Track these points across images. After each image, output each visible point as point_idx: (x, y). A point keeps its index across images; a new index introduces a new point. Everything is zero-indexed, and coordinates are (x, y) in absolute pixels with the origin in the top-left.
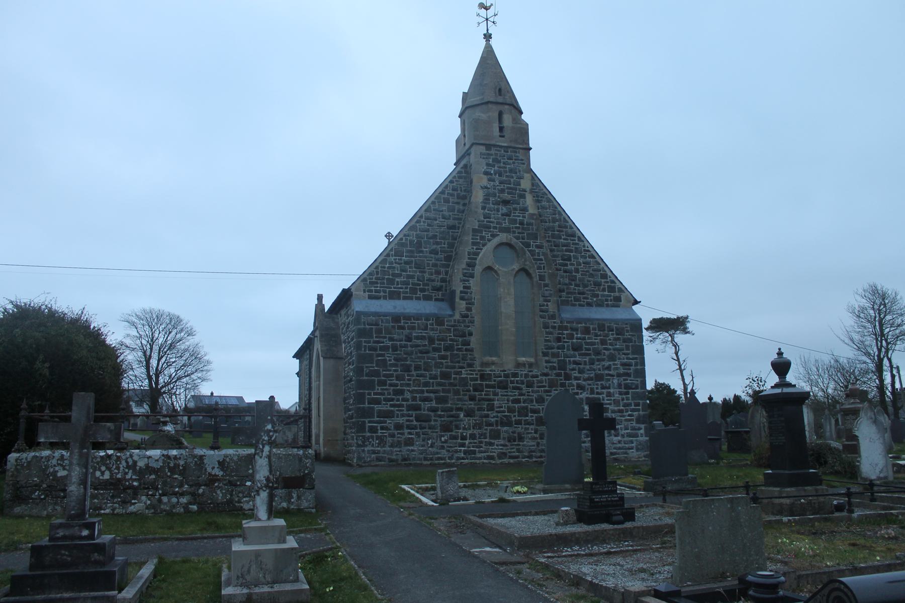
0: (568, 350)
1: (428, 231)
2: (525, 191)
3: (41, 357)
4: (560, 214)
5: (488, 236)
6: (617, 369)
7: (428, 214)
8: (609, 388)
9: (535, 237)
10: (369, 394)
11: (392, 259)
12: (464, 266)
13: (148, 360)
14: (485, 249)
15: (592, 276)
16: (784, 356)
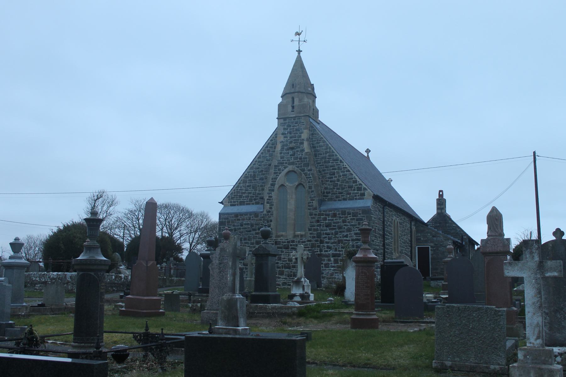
0: (323, 227)
1: (258, 168)
7: (259, 160)
12: (269, 186)
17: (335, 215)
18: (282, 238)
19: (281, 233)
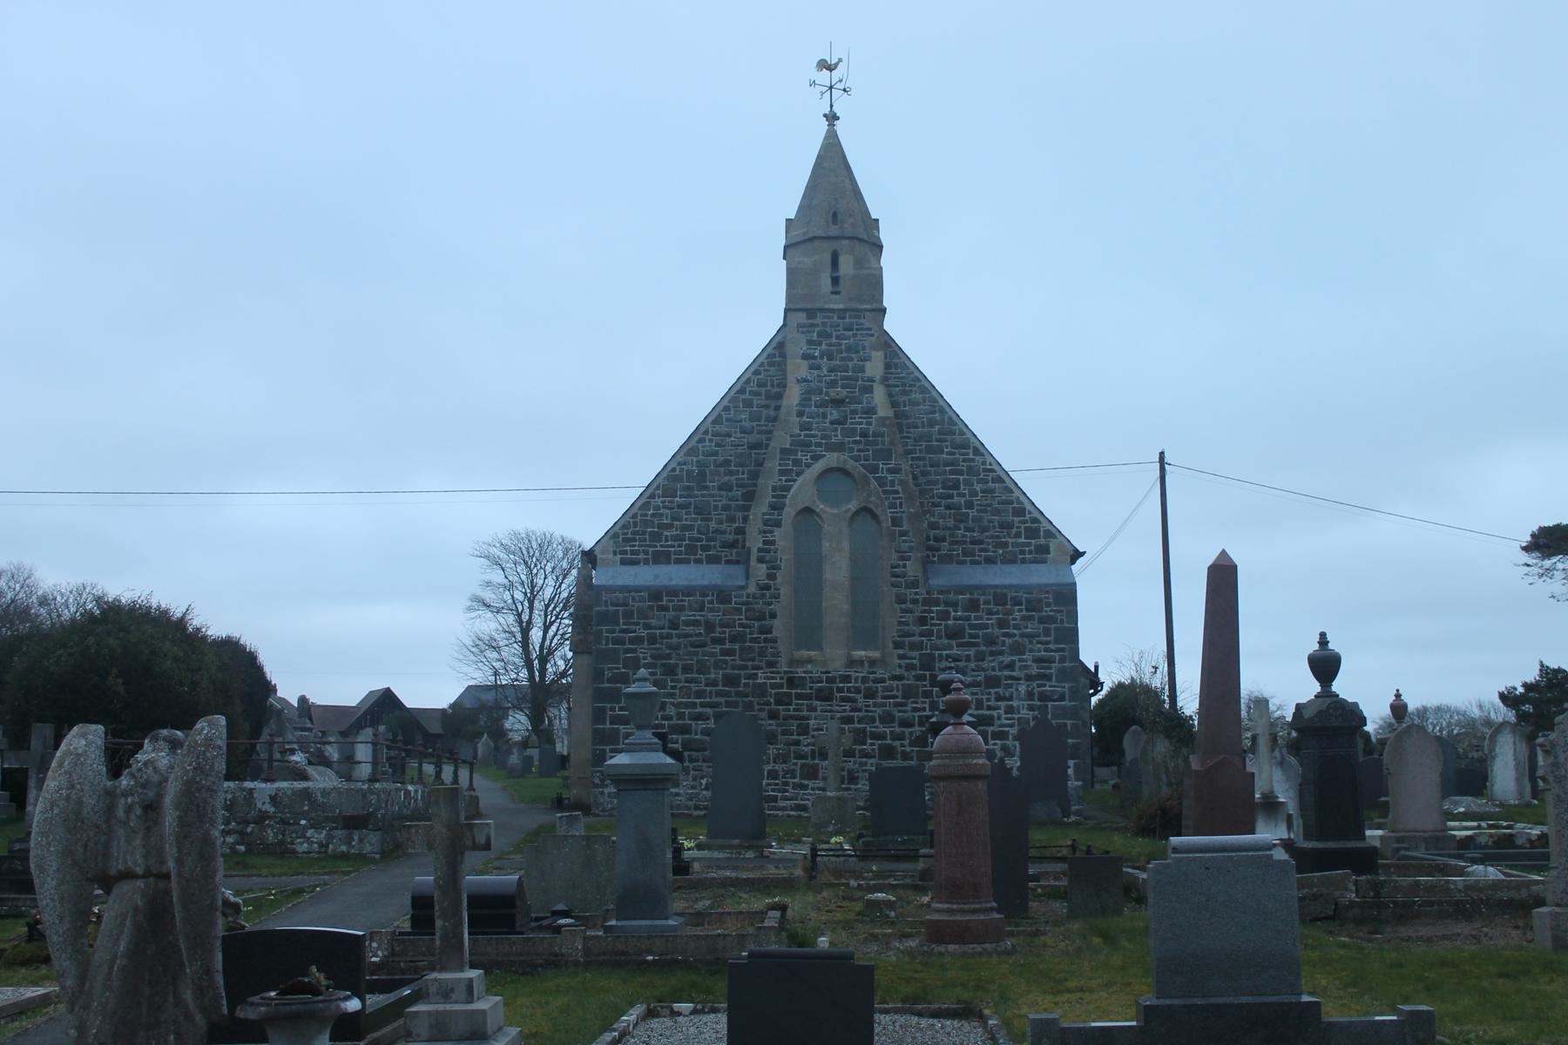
0: (939, 637)
1: (716, 454)
2: (872, 380)
3: (115, 671)
4: (943, 411)
5: (806, 459)
6: (1026, 667)
7: (717, 428)
8: (1010, 698)
9: (887, 455)
10: (612, 709)
11: (659, 501)
12: (765, 509)
13: (526, 631)
14: (800, 480)
15: (997, 512)
16: (1331, 646)
17: (973, 605)
18: (809, 667)
19: (804, 653)
